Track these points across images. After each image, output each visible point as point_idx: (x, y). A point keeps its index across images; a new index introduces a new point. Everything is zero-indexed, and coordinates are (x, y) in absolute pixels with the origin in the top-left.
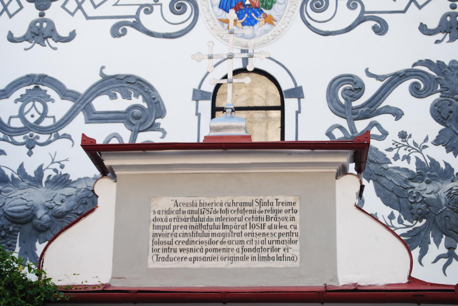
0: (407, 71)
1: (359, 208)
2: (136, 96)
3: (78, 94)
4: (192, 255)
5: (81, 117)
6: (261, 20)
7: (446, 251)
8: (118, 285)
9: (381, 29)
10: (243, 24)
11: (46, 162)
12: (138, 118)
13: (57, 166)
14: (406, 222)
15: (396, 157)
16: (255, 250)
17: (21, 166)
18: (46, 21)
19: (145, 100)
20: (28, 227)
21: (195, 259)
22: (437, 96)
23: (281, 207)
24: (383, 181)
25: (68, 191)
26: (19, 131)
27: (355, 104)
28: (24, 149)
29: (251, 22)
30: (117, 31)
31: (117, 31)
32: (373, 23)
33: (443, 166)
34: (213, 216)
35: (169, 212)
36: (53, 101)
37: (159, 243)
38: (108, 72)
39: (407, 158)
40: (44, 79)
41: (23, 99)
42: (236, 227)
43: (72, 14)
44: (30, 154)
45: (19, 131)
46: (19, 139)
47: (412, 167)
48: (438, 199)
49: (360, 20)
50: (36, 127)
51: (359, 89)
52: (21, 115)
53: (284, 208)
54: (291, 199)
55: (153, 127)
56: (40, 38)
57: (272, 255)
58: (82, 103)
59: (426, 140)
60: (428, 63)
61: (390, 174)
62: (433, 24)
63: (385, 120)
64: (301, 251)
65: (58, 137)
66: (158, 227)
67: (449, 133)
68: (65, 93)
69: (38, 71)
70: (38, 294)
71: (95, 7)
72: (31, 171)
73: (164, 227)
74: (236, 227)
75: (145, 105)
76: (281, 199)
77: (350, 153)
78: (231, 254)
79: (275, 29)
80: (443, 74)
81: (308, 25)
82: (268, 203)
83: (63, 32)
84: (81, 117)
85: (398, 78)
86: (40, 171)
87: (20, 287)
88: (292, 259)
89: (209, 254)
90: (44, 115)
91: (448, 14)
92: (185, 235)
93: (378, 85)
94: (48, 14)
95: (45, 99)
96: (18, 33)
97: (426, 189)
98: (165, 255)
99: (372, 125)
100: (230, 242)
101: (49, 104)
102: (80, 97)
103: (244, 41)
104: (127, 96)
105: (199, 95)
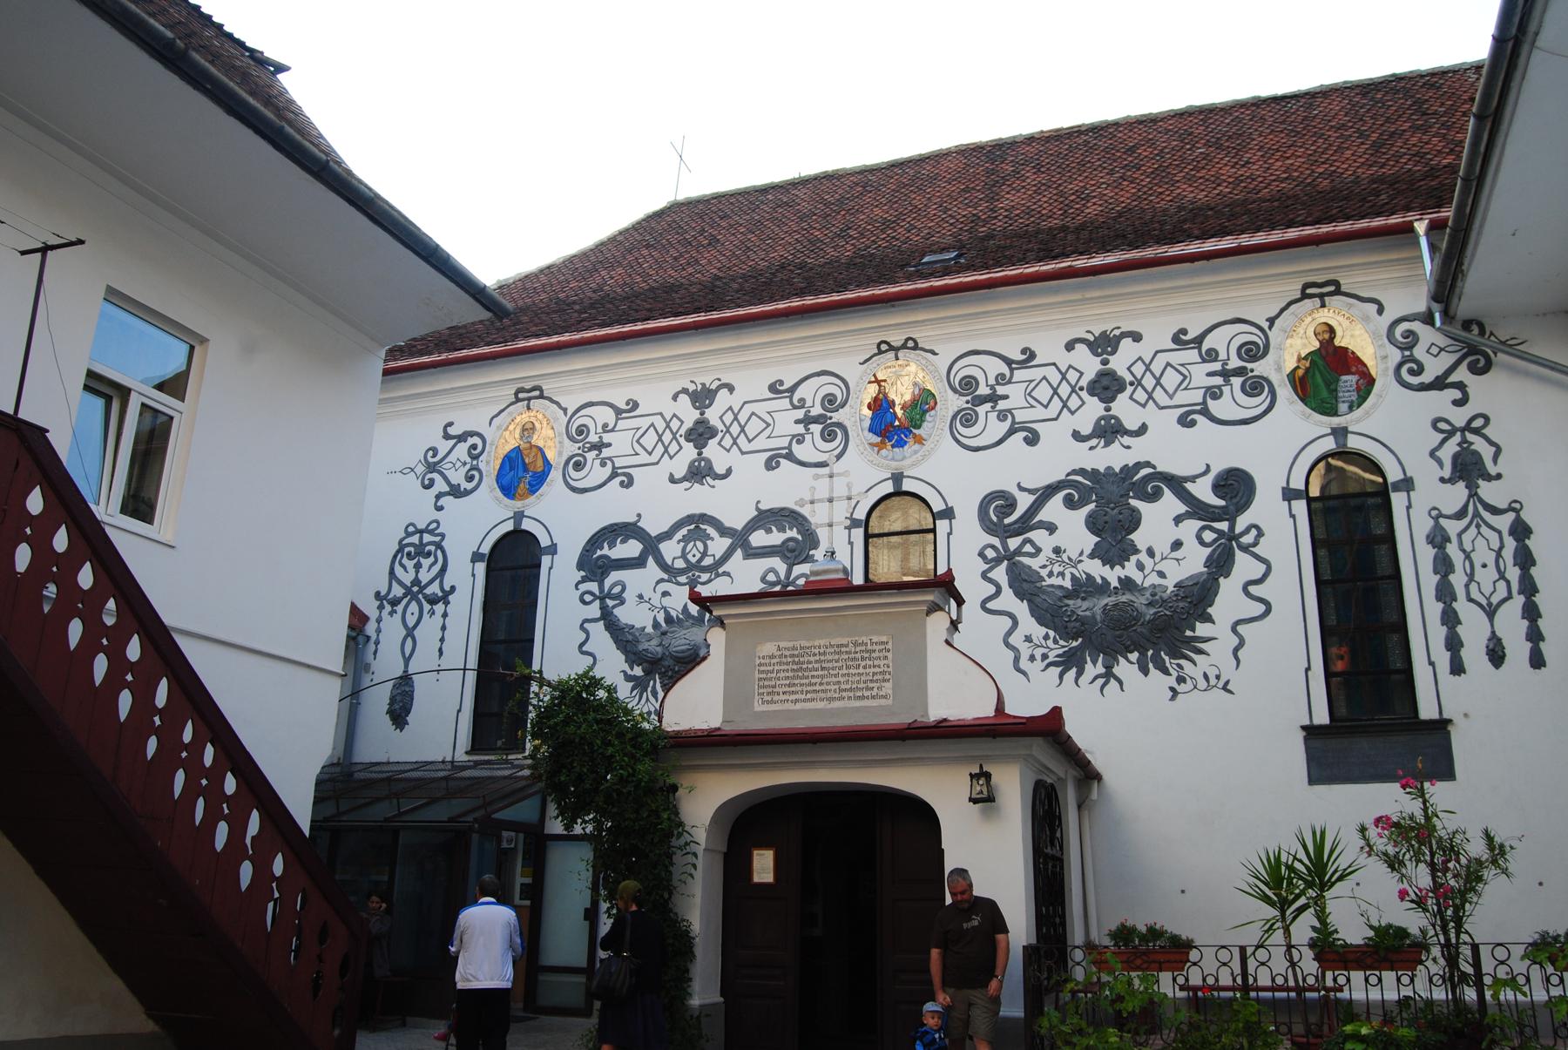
1: (948, 643)
4: (793, 697)
6: (911, 441)
7: (1103, 670)
8: (728, 728)
9: (1033, 439)
12: (793, 551)
14: (1062, 642)
15: (1051, 574)
16: (851, 690)
19: (799, 532)
21: (796, 701)
22: (1092, 506)
24: (1038, 600)
26: (682, 572)
27: (1007, 521)
29: (900, 444)
30: (771, 465)
31: (771, 465)
33: (1099, 581)
35: (772, 657)
38: (763, 507)
39: (1062, 574)
40: (704, 518)
41: (686, 540)
45: (682, 572)
46: (683, 579)
47: (1067, 584)
48: (1094, 616)
49: (1011, 432)
50: (698, 567)
51: (1011, 505)
53: (877, 648)
54: (884, 639)
55: (809, 559)
58: (740, 540)
59: (1081, 554)
60: (1082, 472)
61: (1044, 592)
62: (1086, 430)
63: (1039, 536)
65: (718, 575)
68: (724, 531)
76: (875, 639)
80: (1098, 482)
81: (958, 441)
82: (862, 644)
83: (720, 470)
85: (1049, 491)
88: (885, 697)
90: (704, 554)
91: (1102, 418)
93: (1032, 498)
94: (706, 452)
97: (1081, 607)
102: (1484, 71)
103: (894, 464)
104: (782, 530)
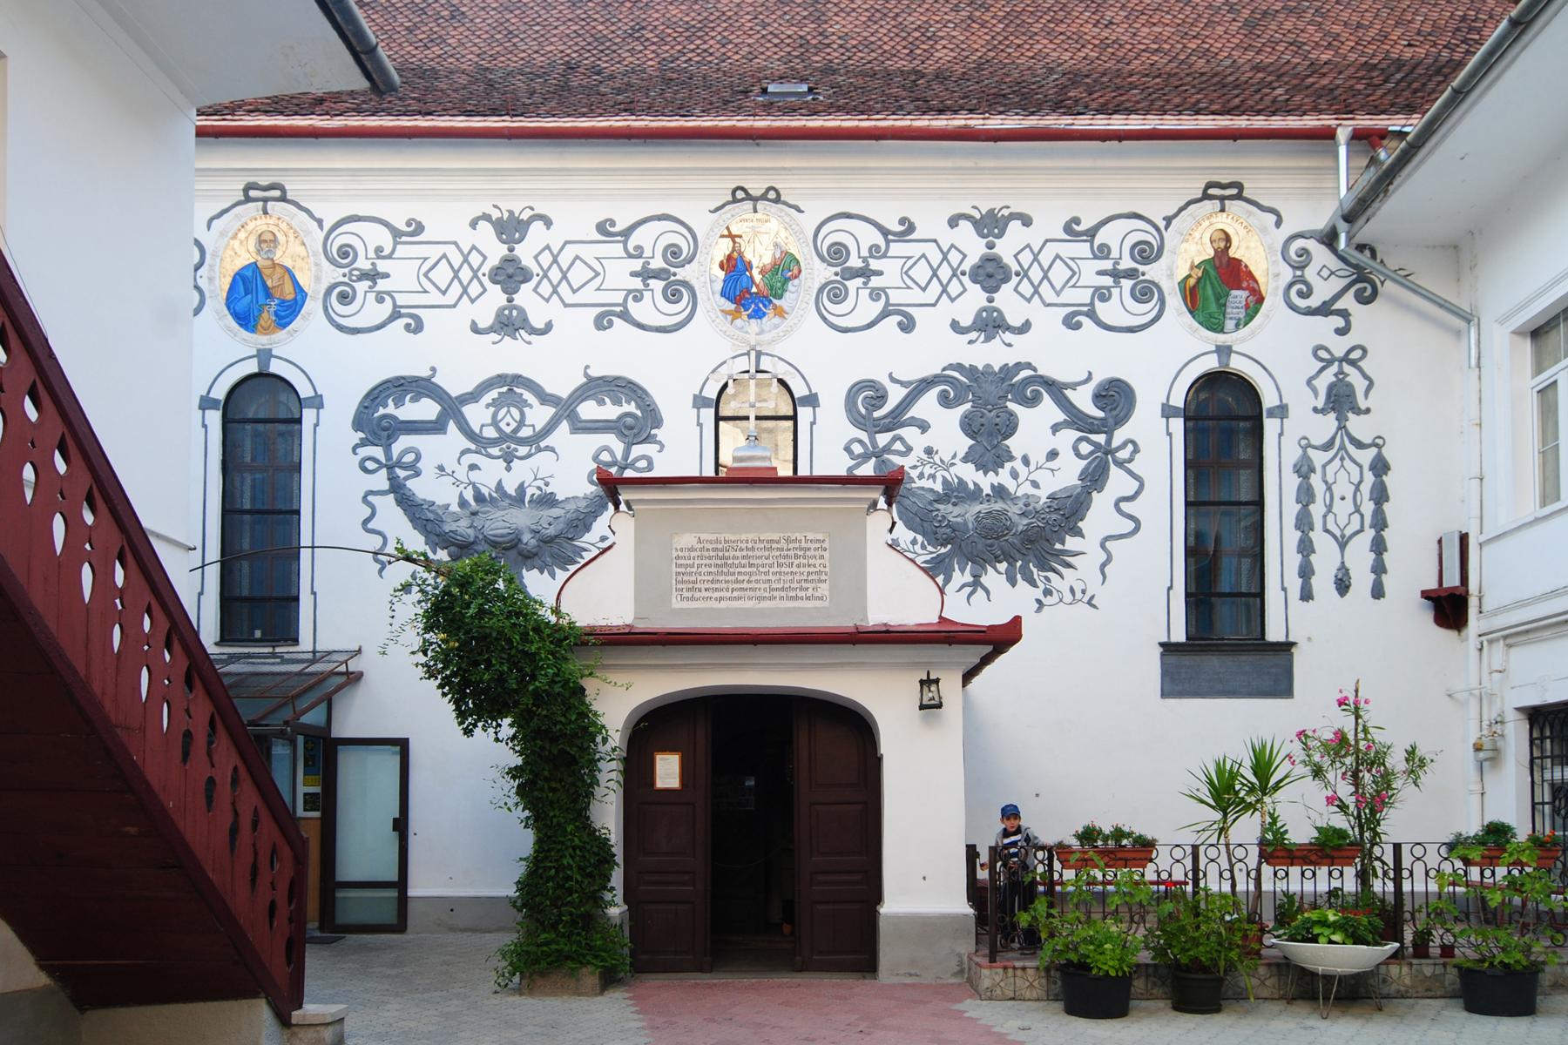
0: (936, 376)
2: (628, 402)
3: (560, 399)
5: (564, 426)
6: (770, 312)
8: (642, 626)
9: (907, 326)
10: (750, 317)
11: (529, 479)
12: (632, 428)
13: (541, 483)
14: (930, 548)
15: (921, 476)
16: (783, 589)
17: (500, 483)
18: (516, 307)
19: (638, 407)
20: (513, 553)
21: (721, 599)
22: (968, 406)
23: (809, 545)
25: (555, 512)
26: (494, 442)
27: (877, 414)
28: (501, 463)
29: (758, 315)
30: (602, 322)
32: (899, 318)
33: (971, 486)
34: (738, 554)
35: (691, 549)
36: (531, 406)
37: (683, 582)
38: (594, 373)
39: (933, 476)
41: (495, 404)
42: (763, 566)
43: (547, 300)
44: (508, 469)
45: (494, 442)
46: (495, 451)
47: (938, 487)
48: (965, 524)
49: (885, 314)
50: (513, 437)
51: (882, 397)
52: (495, 423)
54: (820, 537)
56: (511, 329)
57: (802, 594)
58: (566, 409)
59: (954, 456)
60: (959, 367)
61: (914, 494)
62: (966, 321)
64: (831, 590)
65: (539, 450)
66: (681, 566)
67: (980, 450)
68: (545, 398)
69: (511, 371)
70: (566, 638)
71: (574, 291)
72: (511, 489)
73: (687, 566)
74: (763, 566)
75: (639, 413)
77: (882, 487)
78: (758, 594)
79: (786, 323)
80: (976, 380)
81: (824, 319)
83: (537, 322)
84: (564, 426)
85: (925, 384)
86: (521, 489)
87: (548, 631)
88: (821, 598)
89: (735, 594)
91: (984, 309)
92: (710, 573)
93: (904, 391)
94: (518, 299)
95: (521, 404)
96: (657, 447)
97: (951, 512)
98: (689, 595)
99: (895, 439)
100: (757, 581)
101: (526, 410)
105: (699, 402)
